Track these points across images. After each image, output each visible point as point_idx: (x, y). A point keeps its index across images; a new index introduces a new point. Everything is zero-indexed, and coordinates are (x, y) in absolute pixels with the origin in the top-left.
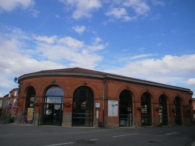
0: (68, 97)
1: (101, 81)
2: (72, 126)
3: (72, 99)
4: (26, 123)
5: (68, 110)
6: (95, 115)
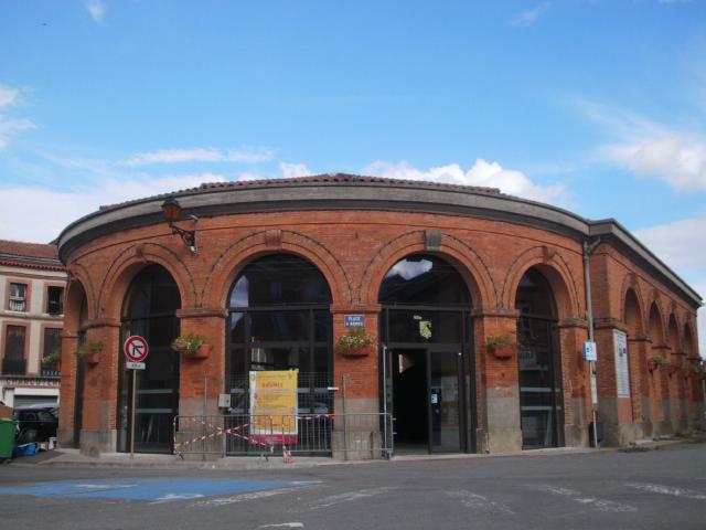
0: (502, 312)
1: (578, 248)
2: (528, 442)
3: (512, 325)
4: (293, 455)
5: (503, 375)
6: (575, 395)
